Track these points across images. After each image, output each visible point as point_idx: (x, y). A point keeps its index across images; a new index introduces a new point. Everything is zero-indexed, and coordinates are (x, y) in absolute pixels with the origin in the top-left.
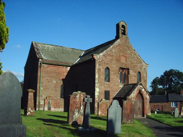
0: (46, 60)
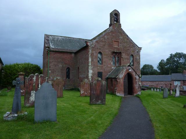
0: (53, 49)
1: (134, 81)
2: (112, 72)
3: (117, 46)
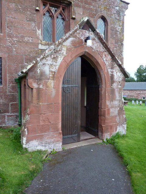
1: (105, 89)
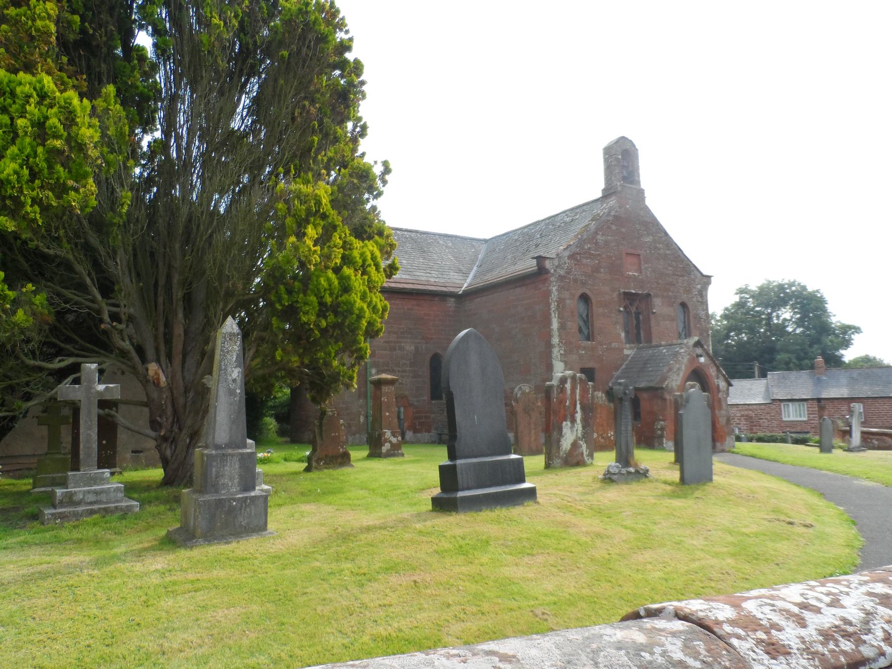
2: (624, 367)
3: (636, 271)
